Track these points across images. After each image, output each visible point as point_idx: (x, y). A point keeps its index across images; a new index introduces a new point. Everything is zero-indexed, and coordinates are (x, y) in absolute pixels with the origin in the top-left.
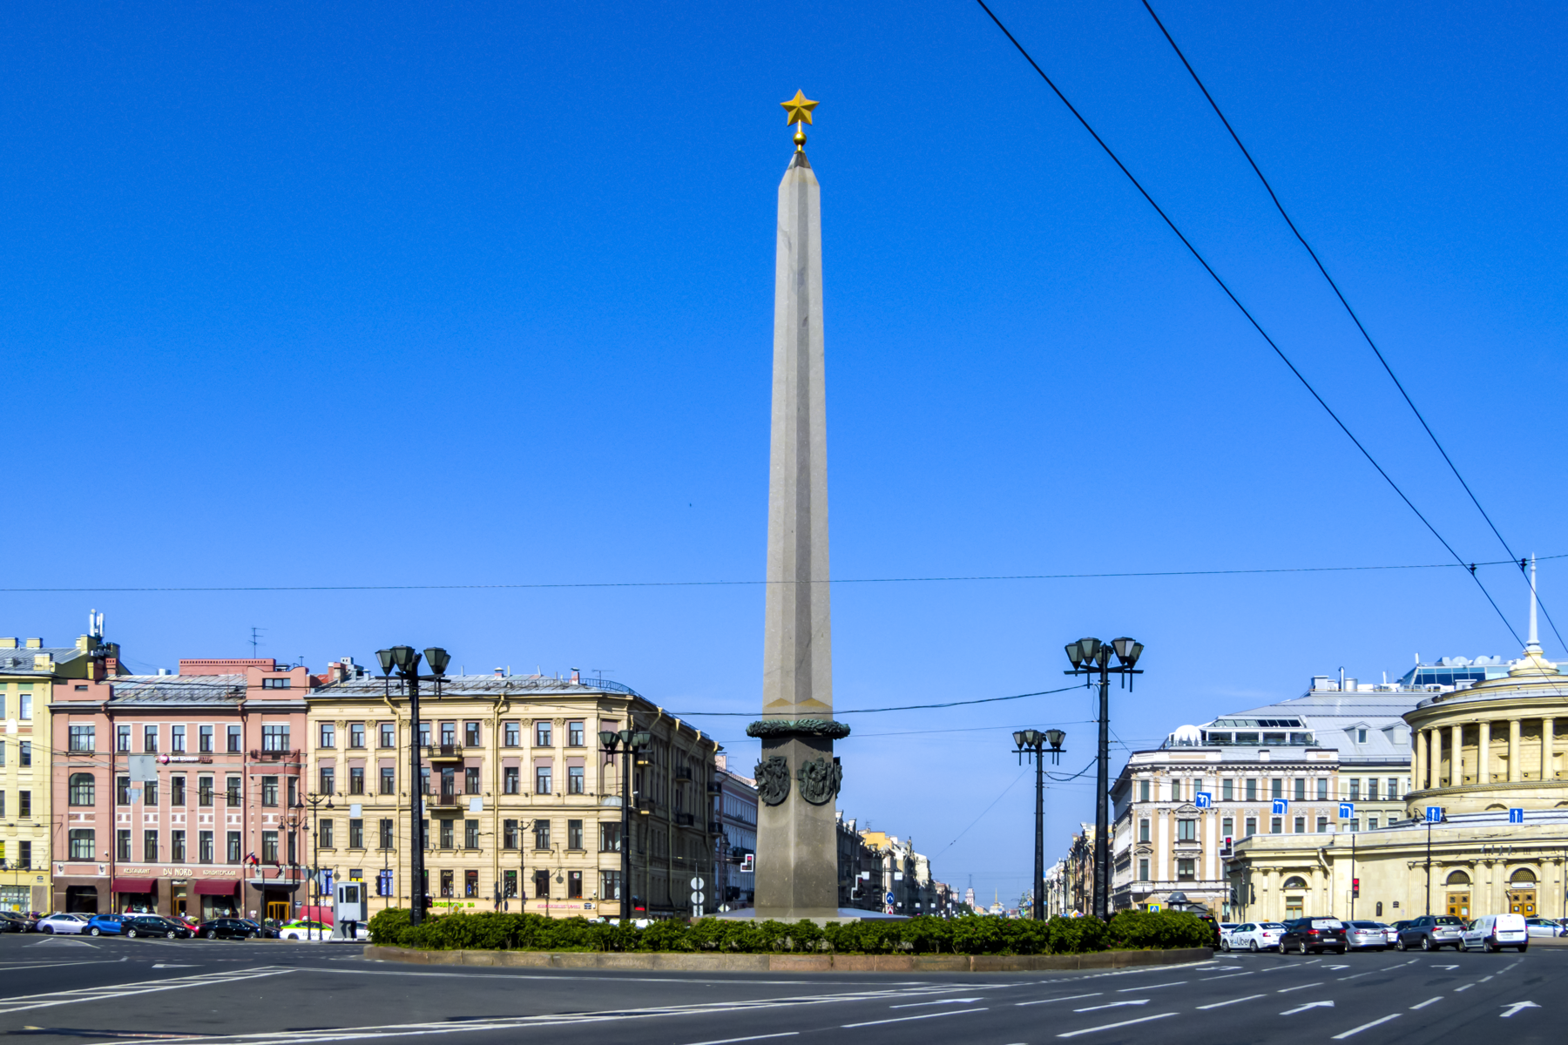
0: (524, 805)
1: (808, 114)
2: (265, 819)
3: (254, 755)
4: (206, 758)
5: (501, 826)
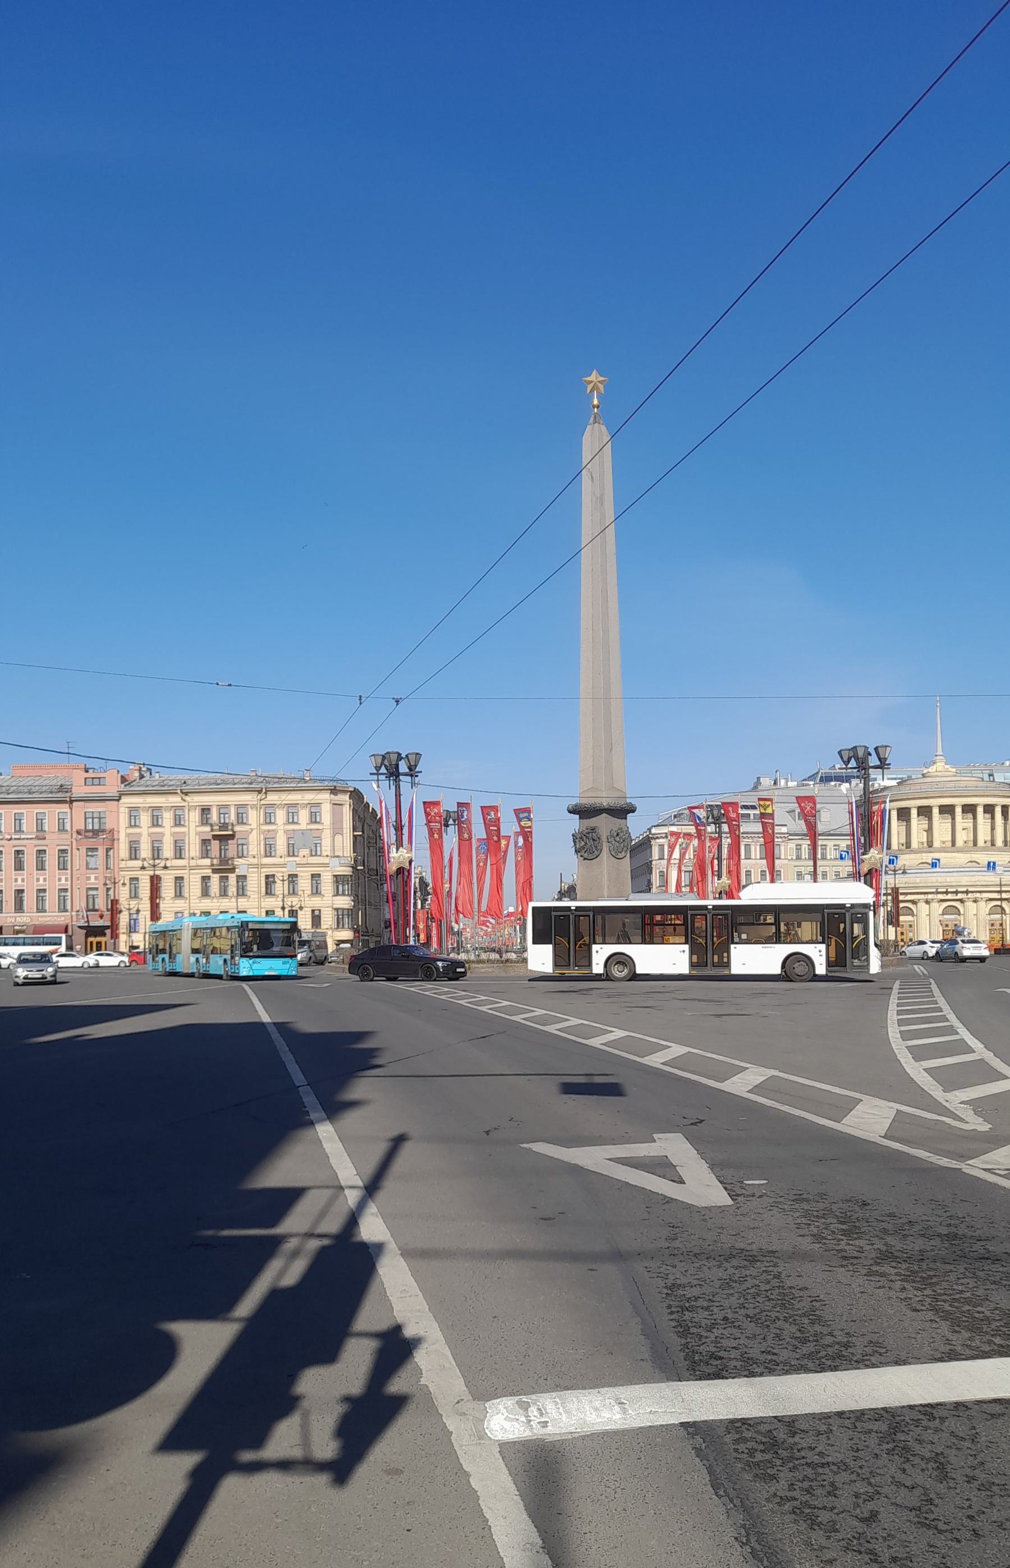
0: (281, 865)
1: (601, 386)
2: (89, 878)
3: (78, 833)
4: (40, 834)
5: (263, 879)
